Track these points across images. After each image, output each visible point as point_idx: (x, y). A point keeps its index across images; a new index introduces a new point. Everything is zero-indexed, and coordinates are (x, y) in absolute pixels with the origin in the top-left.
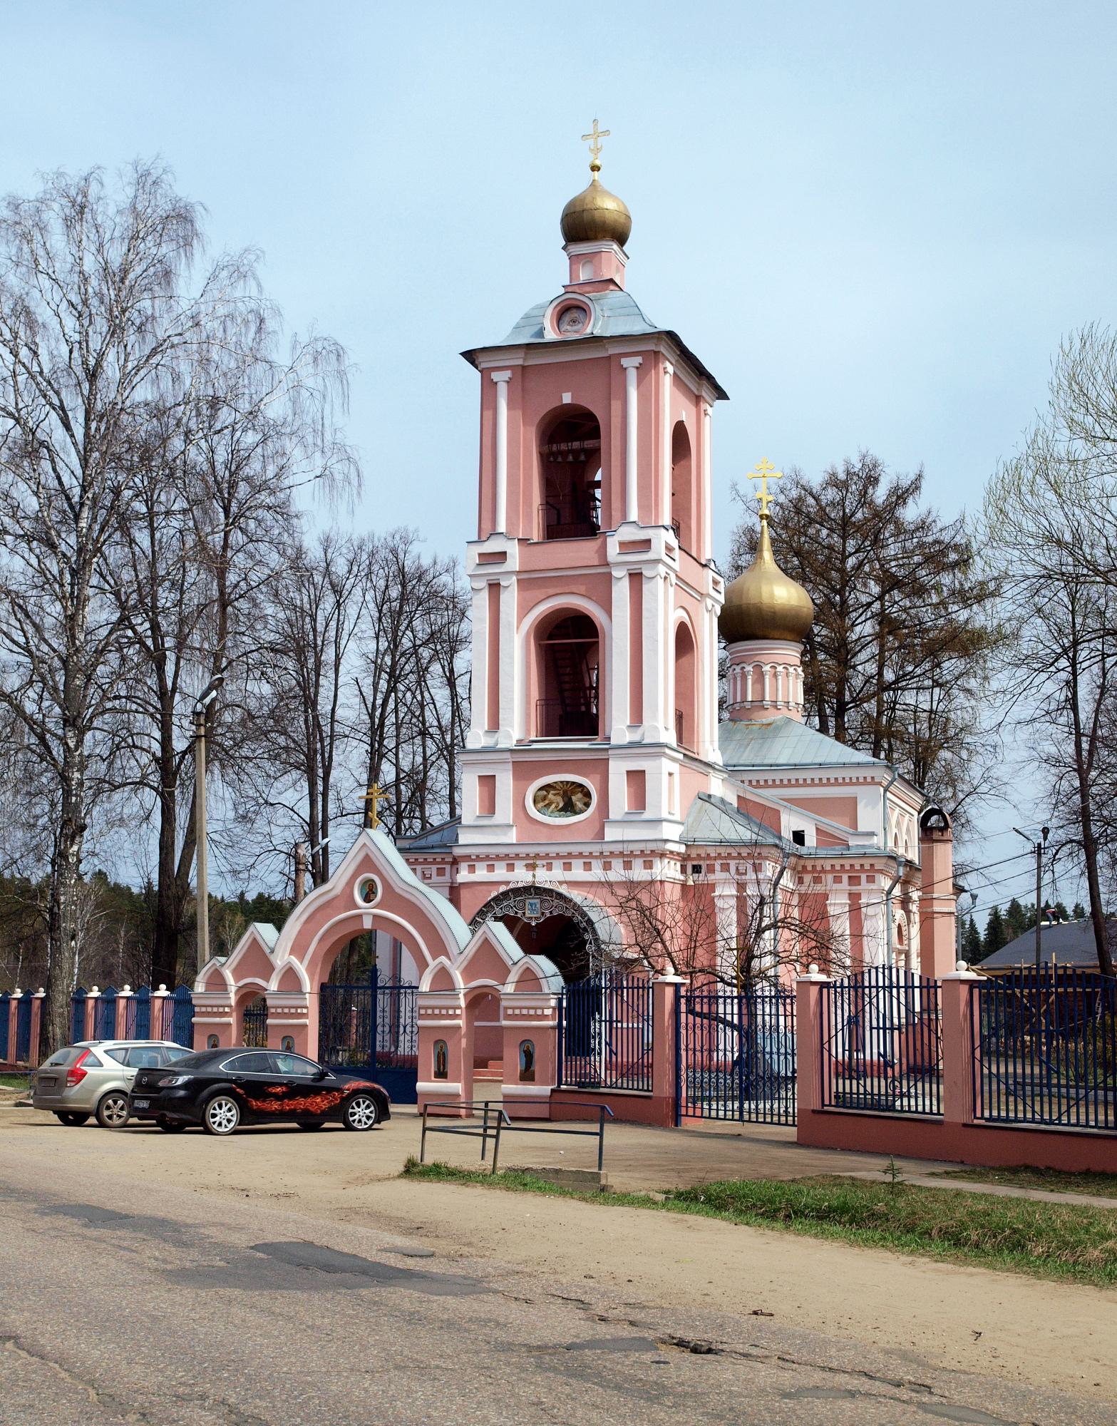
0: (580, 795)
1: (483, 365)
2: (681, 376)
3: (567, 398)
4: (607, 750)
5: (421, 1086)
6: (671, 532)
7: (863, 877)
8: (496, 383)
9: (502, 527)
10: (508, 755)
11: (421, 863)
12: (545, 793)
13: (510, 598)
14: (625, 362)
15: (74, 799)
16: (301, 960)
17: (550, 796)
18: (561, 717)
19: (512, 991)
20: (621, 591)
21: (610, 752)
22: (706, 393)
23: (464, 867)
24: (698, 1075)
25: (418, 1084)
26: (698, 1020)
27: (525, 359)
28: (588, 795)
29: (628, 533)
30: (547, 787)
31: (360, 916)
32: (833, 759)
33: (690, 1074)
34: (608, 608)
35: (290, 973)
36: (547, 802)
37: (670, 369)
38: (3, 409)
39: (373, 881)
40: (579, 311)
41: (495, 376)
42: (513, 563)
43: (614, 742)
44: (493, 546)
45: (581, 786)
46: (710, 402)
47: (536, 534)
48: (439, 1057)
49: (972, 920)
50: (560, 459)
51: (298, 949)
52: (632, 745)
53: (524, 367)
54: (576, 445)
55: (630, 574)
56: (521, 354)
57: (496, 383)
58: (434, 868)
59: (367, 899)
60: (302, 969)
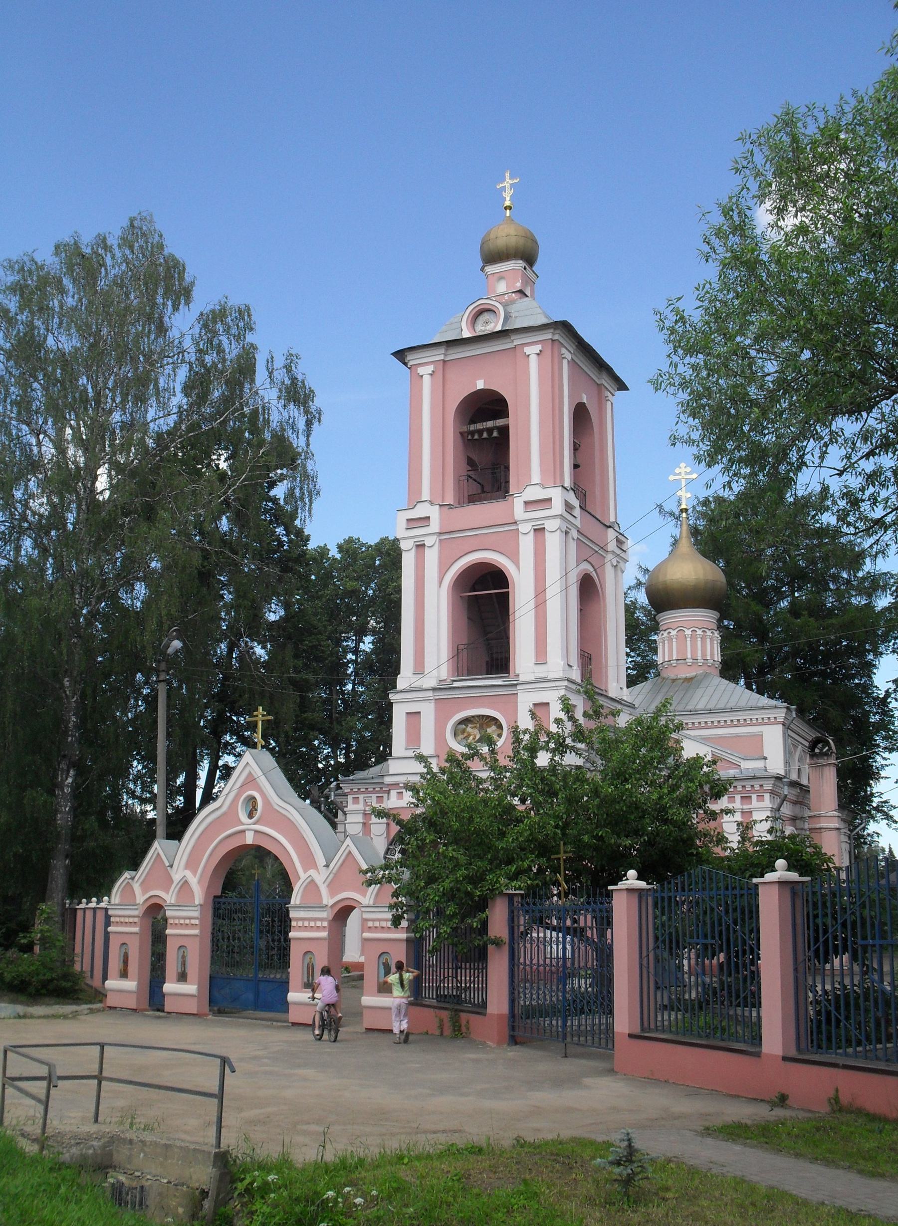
0: (494, 728)
1: (411, 363)
2: (577, 361)
3: (480, 385)
4: (516, 685)
5: (292, 996)
6: (572, 493)
7: (754, 797)
8: (422, 376)
9: (426, 496)
10: (430, 694)
11: (363, 793)
12: (464, 726)
13: (432, 557)
14: (528, 350)
15: (70, 739)
16: (194, 873)
17: (469, 729)
18: (487, 663)
19: (371, 903)
20: (526, 544)
21: (519, 687)
22: (605, 381)
23: (393, 793)
24: (527, 992)
25: (289, 994)
26: (554, 934)
27: (445, 355)
28: (500, 727)
29: (533, 493)
30: (466, 721)
31: (244, 831)
32: (742, 704)
33: (560, 986)
34: (515, 558)
35: (185, 883)
36: (466, 734)
37: (569, 356)
38: (896, 822)
39: (254, 798)
40: (489, 313)
41: (421, 370)
42: (435, 526)
43: (522, 678)
44: (420, 511)
45: (495, 719)
46: (612, 391)
47: (450, 500)
48: (308, 968)
49: (890, 849)
50: (476, 437)
51: (191, 864)
52: (538, 681)
53: (444, 361)
54: (490, 424)
55: (535, 530)
56: (442, 350)
57: (422, 376)
58: (374, 796)
59: (250, 816)
60: (193, 881)
